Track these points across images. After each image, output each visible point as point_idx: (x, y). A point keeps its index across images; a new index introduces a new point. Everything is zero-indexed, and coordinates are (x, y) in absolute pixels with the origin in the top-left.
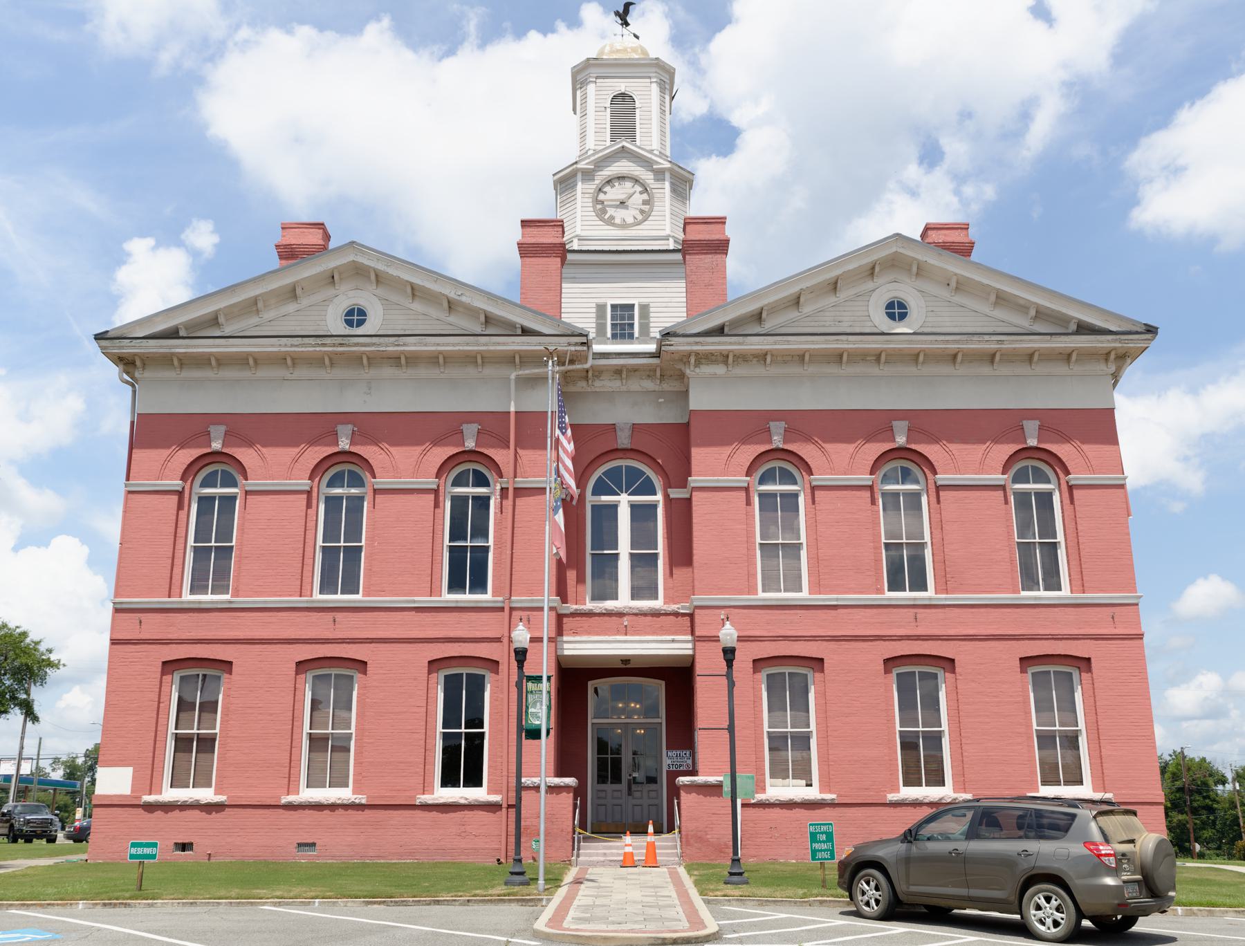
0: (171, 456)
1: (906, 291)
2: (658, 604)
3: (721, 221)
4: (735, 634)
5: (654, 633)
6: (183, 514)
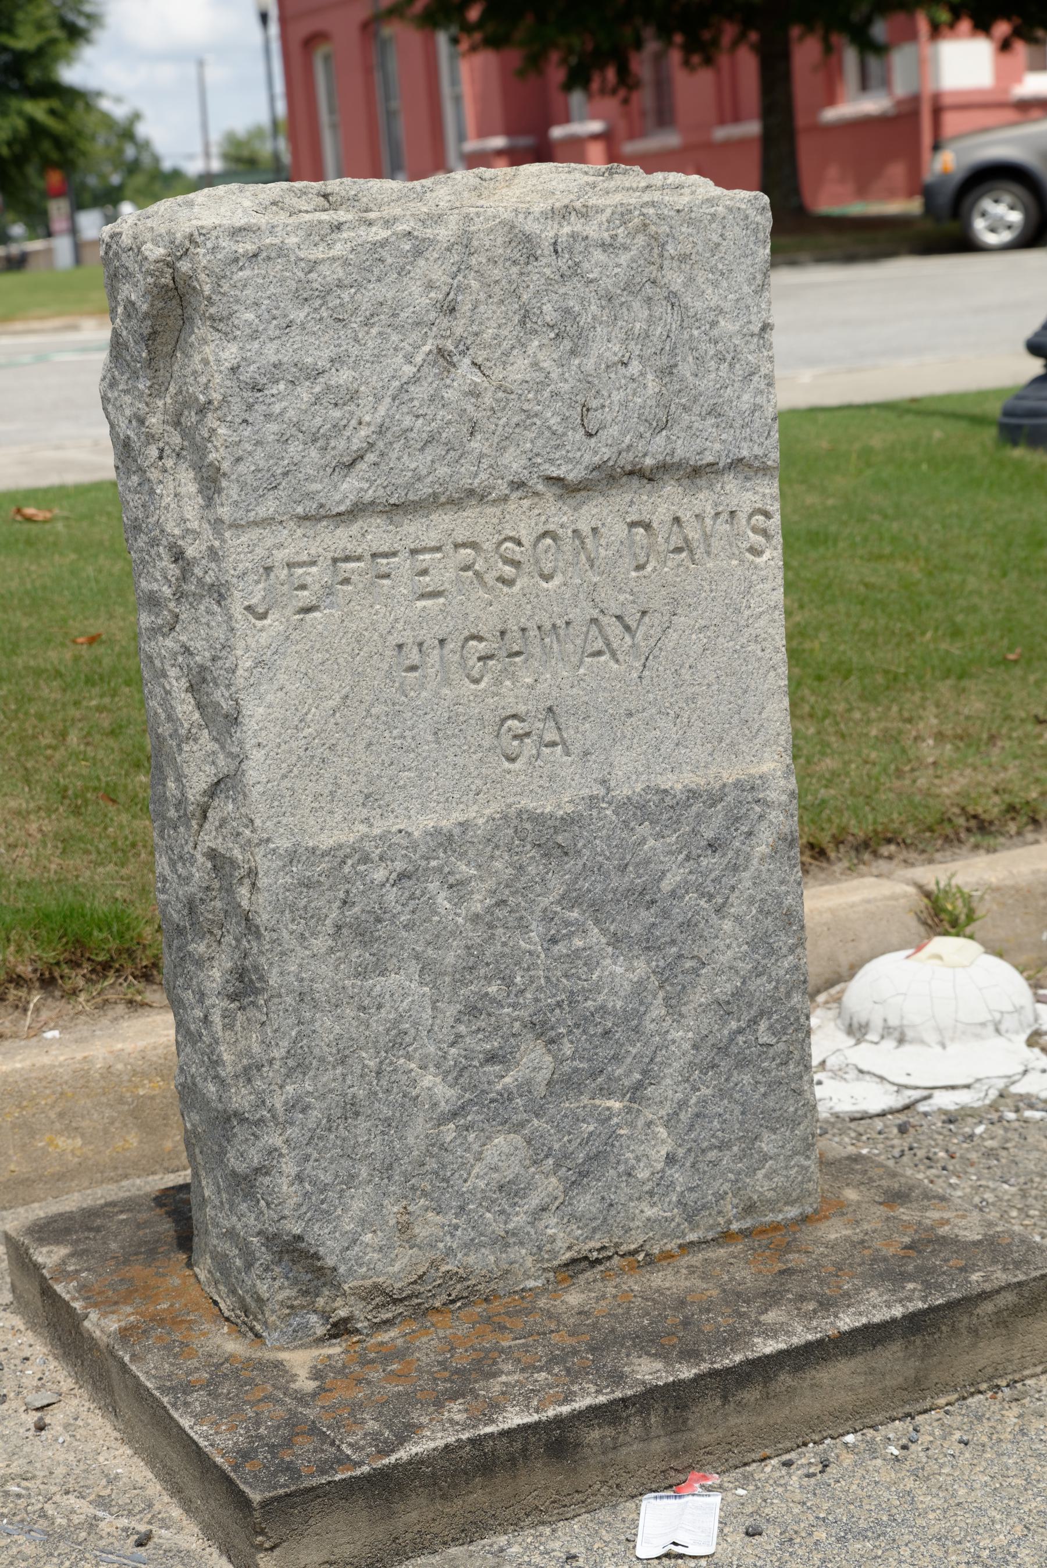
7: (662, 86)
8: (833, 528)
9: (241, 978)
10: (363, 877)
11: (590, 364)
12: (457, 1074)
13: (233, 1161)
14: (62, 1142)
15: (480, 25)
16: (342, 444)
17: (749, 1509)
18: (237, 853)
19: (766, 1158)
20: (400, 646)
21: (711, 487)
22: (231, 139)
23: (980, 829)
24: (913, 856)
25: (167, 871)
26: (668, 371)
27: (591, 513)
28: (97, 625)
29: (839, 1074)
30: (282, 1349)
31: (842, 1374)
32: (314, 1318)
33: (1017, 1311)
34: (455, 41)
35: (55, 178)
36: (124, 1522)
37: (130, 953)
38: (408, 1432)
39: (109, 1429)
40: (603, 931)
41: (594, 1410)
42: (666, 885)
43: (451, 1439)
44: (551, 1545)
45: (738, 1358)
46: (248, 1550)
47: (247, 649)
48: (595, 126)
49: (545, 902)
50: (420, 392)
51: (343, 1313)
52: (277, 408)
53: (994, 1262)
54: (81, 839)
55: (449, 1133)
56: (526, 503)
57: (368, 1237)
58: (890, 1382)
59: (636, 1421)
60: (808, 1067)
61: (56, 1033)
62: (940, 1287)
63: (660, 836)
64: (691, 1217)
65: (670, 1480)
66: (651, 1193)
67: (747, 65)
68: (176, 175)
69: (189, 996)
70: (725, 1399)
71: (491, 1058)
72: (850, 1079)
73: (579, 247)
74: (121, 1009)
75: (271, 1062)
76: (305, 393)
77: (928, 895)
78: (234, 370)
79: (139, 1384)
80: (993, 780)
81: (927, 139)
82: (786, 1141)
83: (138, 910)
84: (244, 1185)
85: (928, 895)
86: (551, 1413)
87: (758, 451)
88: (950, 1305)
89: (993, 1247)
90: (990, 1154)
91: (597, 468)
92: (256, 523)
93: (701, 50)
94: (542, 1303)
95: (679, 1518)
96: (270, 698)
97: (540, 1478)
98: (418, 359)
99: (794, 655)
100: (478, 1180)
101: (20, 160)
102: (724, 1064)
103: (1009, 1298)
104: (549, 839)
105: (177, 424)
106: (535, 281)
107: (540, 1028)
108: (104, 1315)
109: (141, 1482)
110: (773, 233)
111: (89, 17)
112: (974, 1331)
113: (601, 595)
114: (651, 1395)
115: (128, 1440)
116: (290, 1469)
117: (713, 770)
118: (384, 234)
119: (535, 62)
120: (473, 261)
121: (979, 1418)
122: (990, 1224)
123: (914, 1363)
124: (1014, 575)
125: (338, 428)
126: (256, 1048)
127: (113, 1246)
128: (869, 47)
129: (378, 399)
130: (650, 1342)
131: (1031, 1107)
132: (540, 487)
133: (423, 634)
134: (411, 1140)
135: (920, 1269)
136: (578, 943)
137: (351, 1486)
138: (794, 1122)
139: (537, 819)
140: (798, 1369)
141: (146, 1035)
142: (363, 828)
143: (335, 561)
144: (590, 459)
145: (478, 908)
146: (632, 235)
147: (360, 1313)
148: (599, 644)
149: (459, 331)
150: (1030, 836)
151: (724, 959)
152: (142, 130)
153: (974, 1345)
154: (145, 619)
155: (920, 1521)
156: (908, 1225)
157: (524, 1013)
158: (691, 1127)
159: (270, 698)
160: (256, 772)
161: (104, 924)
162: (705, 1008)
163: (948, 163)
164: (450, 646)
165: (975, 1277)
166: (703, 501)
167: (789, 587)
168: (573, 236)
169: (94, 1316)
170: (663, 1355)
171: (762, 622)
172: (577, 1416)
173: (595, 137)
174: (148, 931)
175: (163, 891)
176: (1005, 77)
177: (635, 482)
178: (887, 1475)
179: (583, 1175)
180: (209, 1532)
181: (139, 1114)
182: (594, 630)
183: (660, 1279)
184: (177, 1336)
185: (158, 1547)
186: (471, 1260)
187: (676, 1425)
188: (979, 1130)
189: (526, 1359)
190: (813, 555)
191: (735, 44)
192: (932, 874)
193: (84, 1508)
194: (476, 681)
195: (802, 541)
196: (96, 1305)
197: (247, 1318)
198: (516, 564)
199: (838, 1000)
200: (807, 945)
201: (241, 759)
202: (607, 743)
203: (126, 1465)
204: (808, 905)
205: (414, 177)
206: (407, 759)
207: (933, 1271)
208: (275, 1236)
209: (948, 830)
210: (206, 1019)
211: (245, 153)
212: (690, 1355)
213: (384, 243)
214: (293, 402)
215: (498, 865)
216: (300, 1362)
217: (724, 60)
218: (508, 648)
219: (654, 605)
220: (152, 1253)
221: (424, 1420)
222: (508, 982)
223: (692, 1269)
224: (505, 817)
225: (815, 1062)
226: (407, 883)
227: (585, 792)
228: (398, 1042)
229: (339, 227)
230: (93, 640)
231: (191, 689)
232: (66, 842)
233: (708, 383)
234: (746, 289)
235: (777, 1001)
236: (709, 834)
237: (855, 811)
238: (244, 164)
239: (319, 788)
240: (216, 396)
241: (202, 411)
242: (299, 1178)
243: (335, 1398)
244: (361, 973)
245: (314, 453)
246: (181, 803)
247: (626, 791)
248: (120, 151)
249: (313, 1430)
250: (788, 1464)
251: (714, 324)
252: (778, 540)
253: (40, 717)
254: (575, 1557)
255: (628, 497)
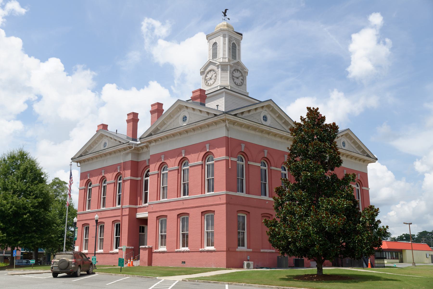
0: (176, 159)
1: (185, 113)
4: (77, 220)
6: (203, 170)
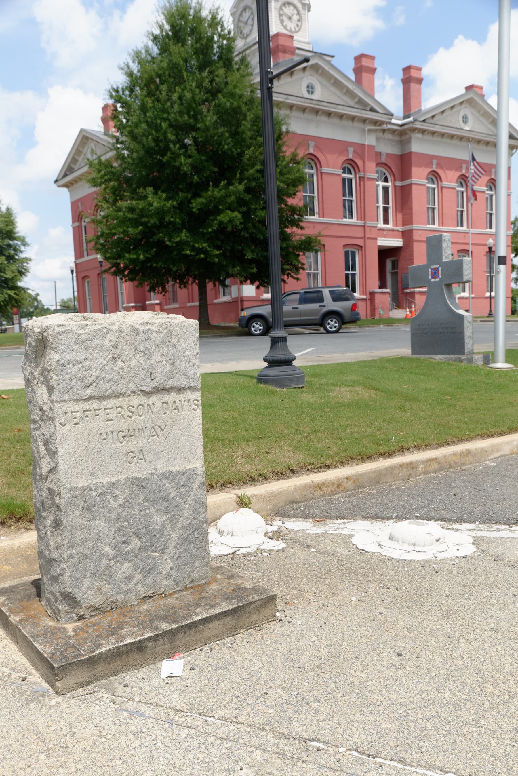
2: (390, 226)
3: (372, 58)
5: (392, 238)
7: (174, 292)
8: (216, 403)
9: (56, 522)
10: (90, 494)
11: (152, 362)
12: (114, 547)
13: (52, 572)
14: (5, 567)
15: (127, 276)
16: (86, 381)
17: (191, 663)
18: (55, 489)
19: (197, 567)
20: (101, 434)
21: (183, 393)
22: (63, 301)
23: (252, 480)
24: (235, 487)
25: (36, 494)
26: (172, 364)
27: (152, 399)
28: (20, 427)
29: (217, 544)
30: (65, 624)
31: (216, 624)
32: (74, 615)
33: (261, 606)
34: (121, 279)
35: (15, 310)
36: (19, 674)
37: (26, 515)
38: (99, 646)
39: (15, 648)
40: (154, 508)
41: (150, 638)
42: (171, 496)
43: (111, 647)
44: (138, 675)
45: (188, 622)
46: (54, 681)
47: (60, 434)
48: (158, 302)
49: (139, 501)
50: (108, 368)
51: (82, 613)
52: (69, 371)
53: (255, 593)
54: (14, 484)
55: (112, 563)
56: (135, 397)
57: (89, 592)
58: (228, 627)
59: (161, 640)
60: (208, 543)
61: (4, 537)
62: (241, 601)
63: (169, 483)
64: (177, 583)
65: (170, 655)
66: (166, 578)
67: (196, 288)
68: (48, 309)
69: (41, 527)
70: (185, 633)
71: (124, 543)
72: (218, 545)
73: (150, 332)
74: (23, 530)
75: (63, 545)
76: (77, 367)
77: (239, 497)
78: (58, 361)
79: (24, 635)
80: (255, 468)
81: (240, 309)
82: (202, 563)
83: (29, 503)
84: (55, 579)
85: (239, 497)
86: (138, 639)
87: (195, 384)
88: (244, 606)
89: (255, 590)
90: (255, 565)
91: (154, 388)
92: (63, 401)
93: (184, 284)
94: (137, 608)
95: (173, 667)
96: (65, 447)
97: (135, 657)
98: (107, 359)
99: (205, 435)
100: (120, 576)
101: (6, 306)
102: (186, 543)
103: (259, 603)
104: (140, 484)
105: (42, 375)
106: (139, 340)
107: (137, 534)
108: (15, 616)
109: (24, 663)
110: (200, 329)
111: (25, 270)
112: (250, 612)
113: (155, 421)
114: (166, 632)
115: (21, 651)
116: (66, 657)
117: (183, 466)
118: (99, 327)
119: (141, 284)
120: (122, 335)
121: (251, 635)
122: (254, 584)
123: (234, 621)
124: (260, 416)
125: (86, 377)
126: (60, 541)
127: (18, 596)
128: (225, 286)
129: (97, 369)
130: (165, 618)
131: (265, 552)
132: (139, 393)
133: (107, 430)
134: (102, 565)
135: (236, 596)
136: (148, 511)
137: (83, 661)
138: (204, 558)
139: (137, 479)
140: (204, 624)
141: (30, 537)
142: (90, 482)
143: (84, 411)
144: (152, 386)
145: (121, 502)
146: (164, 329)
147: (87, 614)
148: (154, 433)
149: (118, 352)
150: (265, 482)
151: (186, 515)
152: (39, 298)
153: (250, 616)
154: (32, 426)
155: (236, 664)
156: (233, 584)
157: (133, 531)
158: (177, 560)
159: (65, 447)
160: (61, 466)
161: (19, 507)
162: (181, 528)
163: (245, 313)
164: (115, 433)
165: (250, 598)
166: (182, 397)
167: (204, 418)
168: (148, 329)
169: (12, 616)
170: (169, 622)
171: (196, 428)
172: (145, 639)
173: (157, 304)
174: (31, 509)
175: (35, 499)
176: (258, 294)
177: (164, 392)
178: (227, 652)
179: (148, 573)
180: (43, 676)
181: (27, 559)
182: (153, 429)
183: (169, 601)
184: (35, 621)
185: (28, 681)
186: (117, 597)
187: (172, 641)
188: (252, 558)
189: (132, 624)
190: (211, 410)
191: (192, 283)
192: (240, 492)
193: (7, 671)
194: (122, 443)
195: (207, 407)
196: (13, 613)
197: (56, 615)
198: (132, 412)
199: (216, 525)
200: (208, 511)
201: (57, 463)
202: (156, 459)
203: (20, 658)
204: (208, 501)
205: (110, 313)
206: (103, 463)
207: (239, 596)
208: (64, 593)
209: (244, 481)
210: (46, 534)
211: (66, 305)
212: (176, 621)
213: (99, 330)
214: (74, 370)
215: (126, 491)
216: (70, 627)
217: (190, 287)
218: (130, 434)
219: (169, 423)
220: (29, 598)
221: (104, 642)
222: (129, 522)
223: (177, 598)
224: (129, 478)
225: (210, 541)
226: (102, 496)
227: (150, 472)
228: (99, 539)
229: (87, 325)
230: (19, 430)
231: (44, 444)
232: (9, 485)
233: (182, 367)
234: (193, 344)
235: (200, 526)
236: (182, 483)
237: (221, 475)
238: (65, 308)
239: (78, 471)
240: (53, 368)
241: (49, 372)
242: (71, 576)
243: (79, 637)
244: (89, 520)
245: (79, 383)
246: (41, 475)
247: (161, 472)
248: (33, 303)
249: (73, 646)
250: (201, 650)
251: (184, 352)
252: (201, 407)
253: (4, 451)
254: (144, 678)
255: (162, 396)
